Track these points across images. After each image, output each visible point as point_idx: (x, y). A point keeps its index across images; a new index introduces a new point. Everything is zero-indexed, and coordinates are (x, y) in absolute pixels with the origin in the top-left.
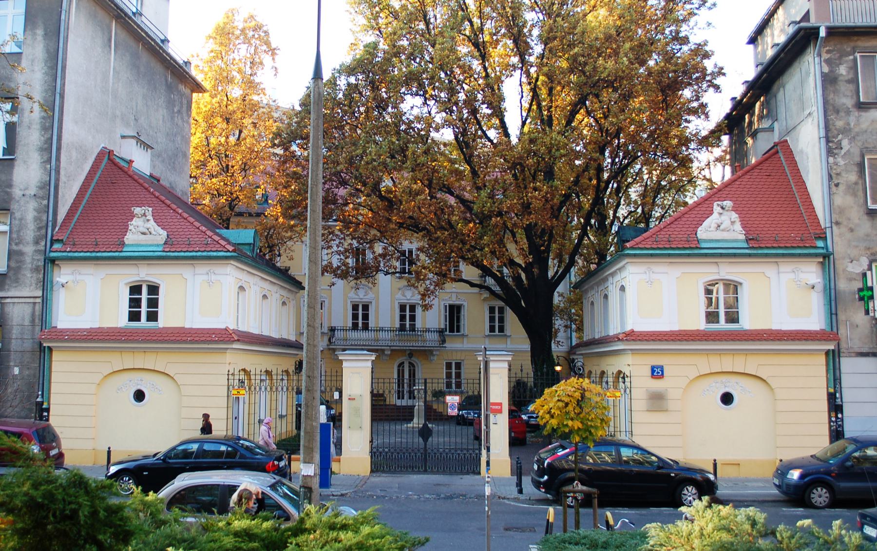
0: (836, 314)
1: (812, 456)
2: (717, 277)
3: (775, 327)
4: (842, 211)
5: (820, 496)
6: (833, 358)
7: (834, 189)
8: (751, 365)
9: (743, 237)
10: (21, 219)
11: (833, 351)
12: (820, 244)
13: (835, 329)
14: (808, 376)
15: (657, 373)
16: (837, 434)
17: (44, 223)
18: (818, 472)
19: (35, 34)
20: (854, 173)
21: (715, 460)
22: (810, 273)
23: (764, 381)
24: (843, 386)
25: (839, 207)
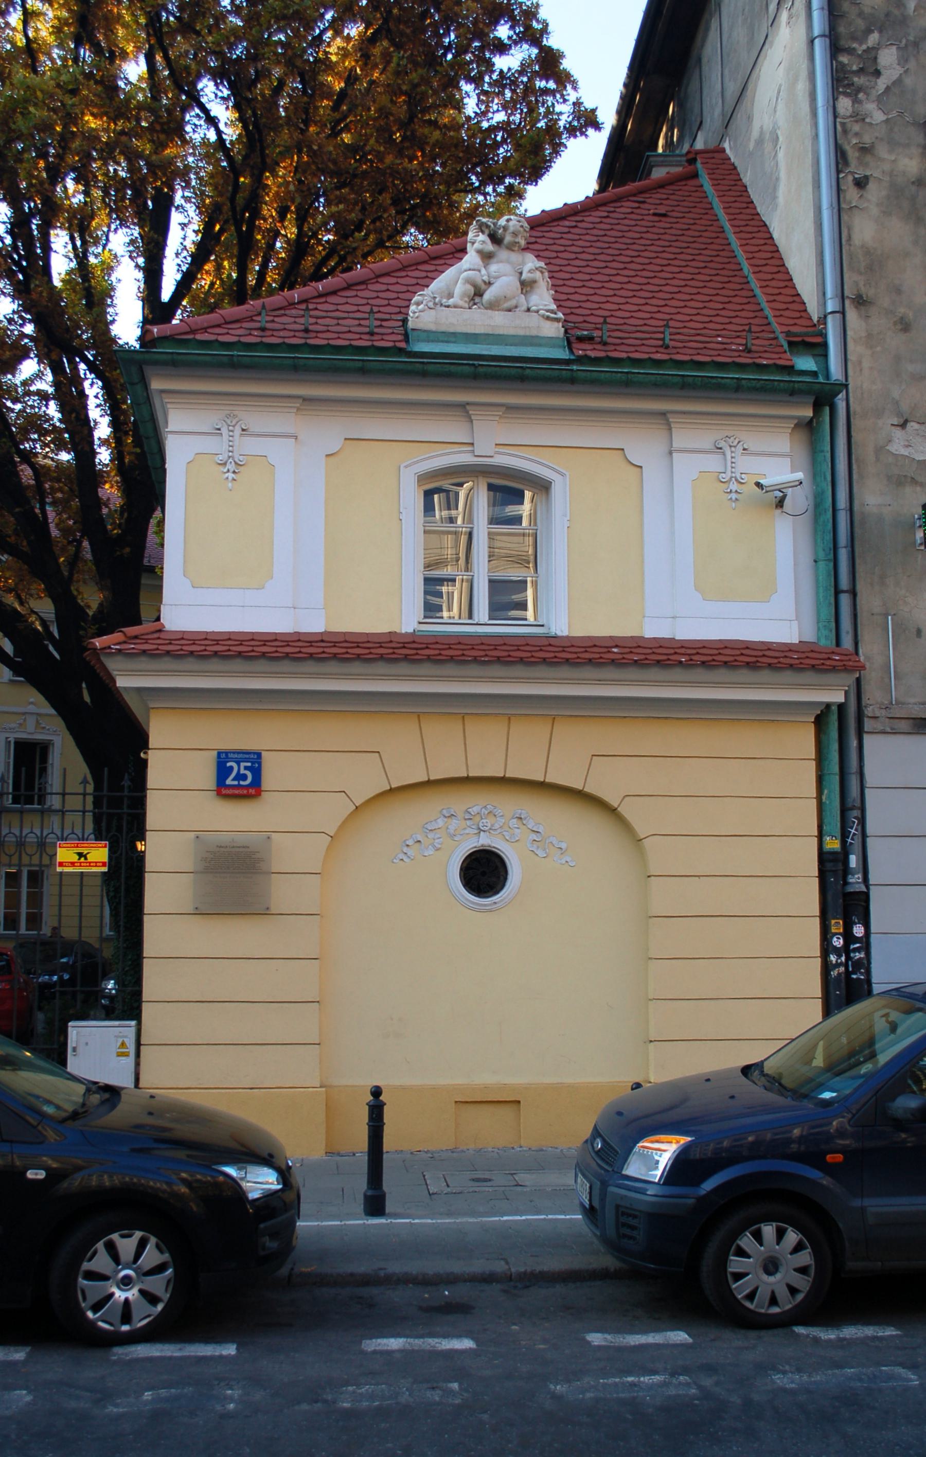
0: (853, 593)
1: (746, 1070)
2: (464, 458)
3: (654, 630)
4: (874, 263)
5: (771, 1266)
6: (840, 734)
7: (852, 193)
8: (567, 754)
9: (554, 330)
11: (841, 707)
12: (806, 363)
13: (847, 642)
14: (750, 805)
15: (239, 778)
16: (845, 986)
18: (777, 1148)
20: (916, 151)
21: (377, 1092)
22: (773, 457)
23: (611, 811)
24: (870, 830)
25: (868, 252)
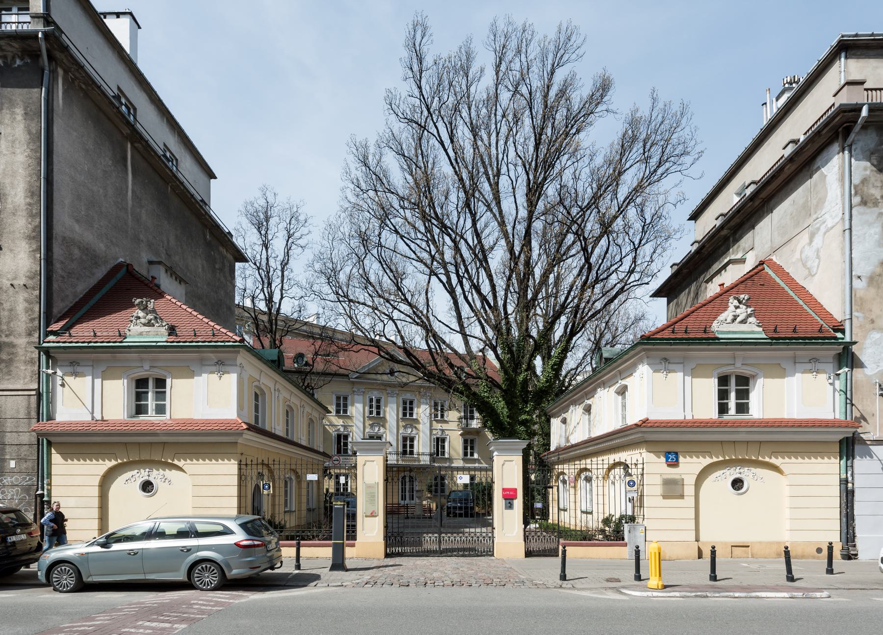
10: (11, 310)
17: (36, 315)
19: (13, 113)
